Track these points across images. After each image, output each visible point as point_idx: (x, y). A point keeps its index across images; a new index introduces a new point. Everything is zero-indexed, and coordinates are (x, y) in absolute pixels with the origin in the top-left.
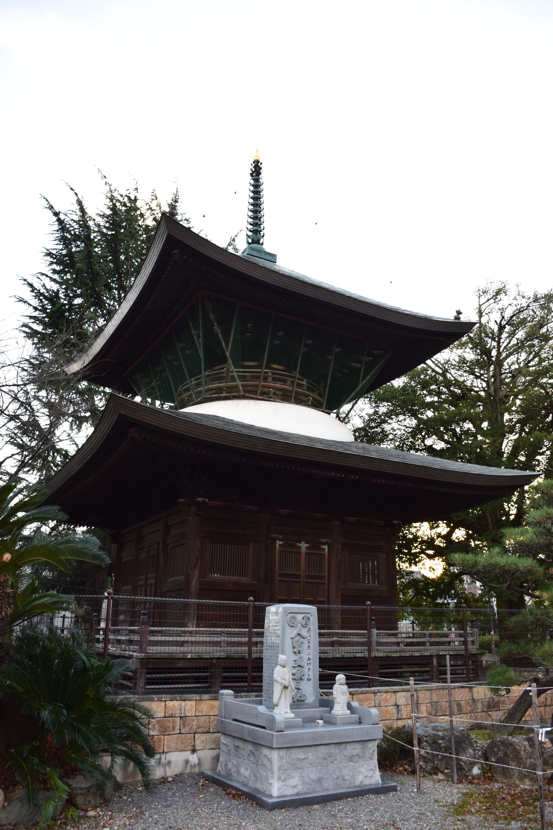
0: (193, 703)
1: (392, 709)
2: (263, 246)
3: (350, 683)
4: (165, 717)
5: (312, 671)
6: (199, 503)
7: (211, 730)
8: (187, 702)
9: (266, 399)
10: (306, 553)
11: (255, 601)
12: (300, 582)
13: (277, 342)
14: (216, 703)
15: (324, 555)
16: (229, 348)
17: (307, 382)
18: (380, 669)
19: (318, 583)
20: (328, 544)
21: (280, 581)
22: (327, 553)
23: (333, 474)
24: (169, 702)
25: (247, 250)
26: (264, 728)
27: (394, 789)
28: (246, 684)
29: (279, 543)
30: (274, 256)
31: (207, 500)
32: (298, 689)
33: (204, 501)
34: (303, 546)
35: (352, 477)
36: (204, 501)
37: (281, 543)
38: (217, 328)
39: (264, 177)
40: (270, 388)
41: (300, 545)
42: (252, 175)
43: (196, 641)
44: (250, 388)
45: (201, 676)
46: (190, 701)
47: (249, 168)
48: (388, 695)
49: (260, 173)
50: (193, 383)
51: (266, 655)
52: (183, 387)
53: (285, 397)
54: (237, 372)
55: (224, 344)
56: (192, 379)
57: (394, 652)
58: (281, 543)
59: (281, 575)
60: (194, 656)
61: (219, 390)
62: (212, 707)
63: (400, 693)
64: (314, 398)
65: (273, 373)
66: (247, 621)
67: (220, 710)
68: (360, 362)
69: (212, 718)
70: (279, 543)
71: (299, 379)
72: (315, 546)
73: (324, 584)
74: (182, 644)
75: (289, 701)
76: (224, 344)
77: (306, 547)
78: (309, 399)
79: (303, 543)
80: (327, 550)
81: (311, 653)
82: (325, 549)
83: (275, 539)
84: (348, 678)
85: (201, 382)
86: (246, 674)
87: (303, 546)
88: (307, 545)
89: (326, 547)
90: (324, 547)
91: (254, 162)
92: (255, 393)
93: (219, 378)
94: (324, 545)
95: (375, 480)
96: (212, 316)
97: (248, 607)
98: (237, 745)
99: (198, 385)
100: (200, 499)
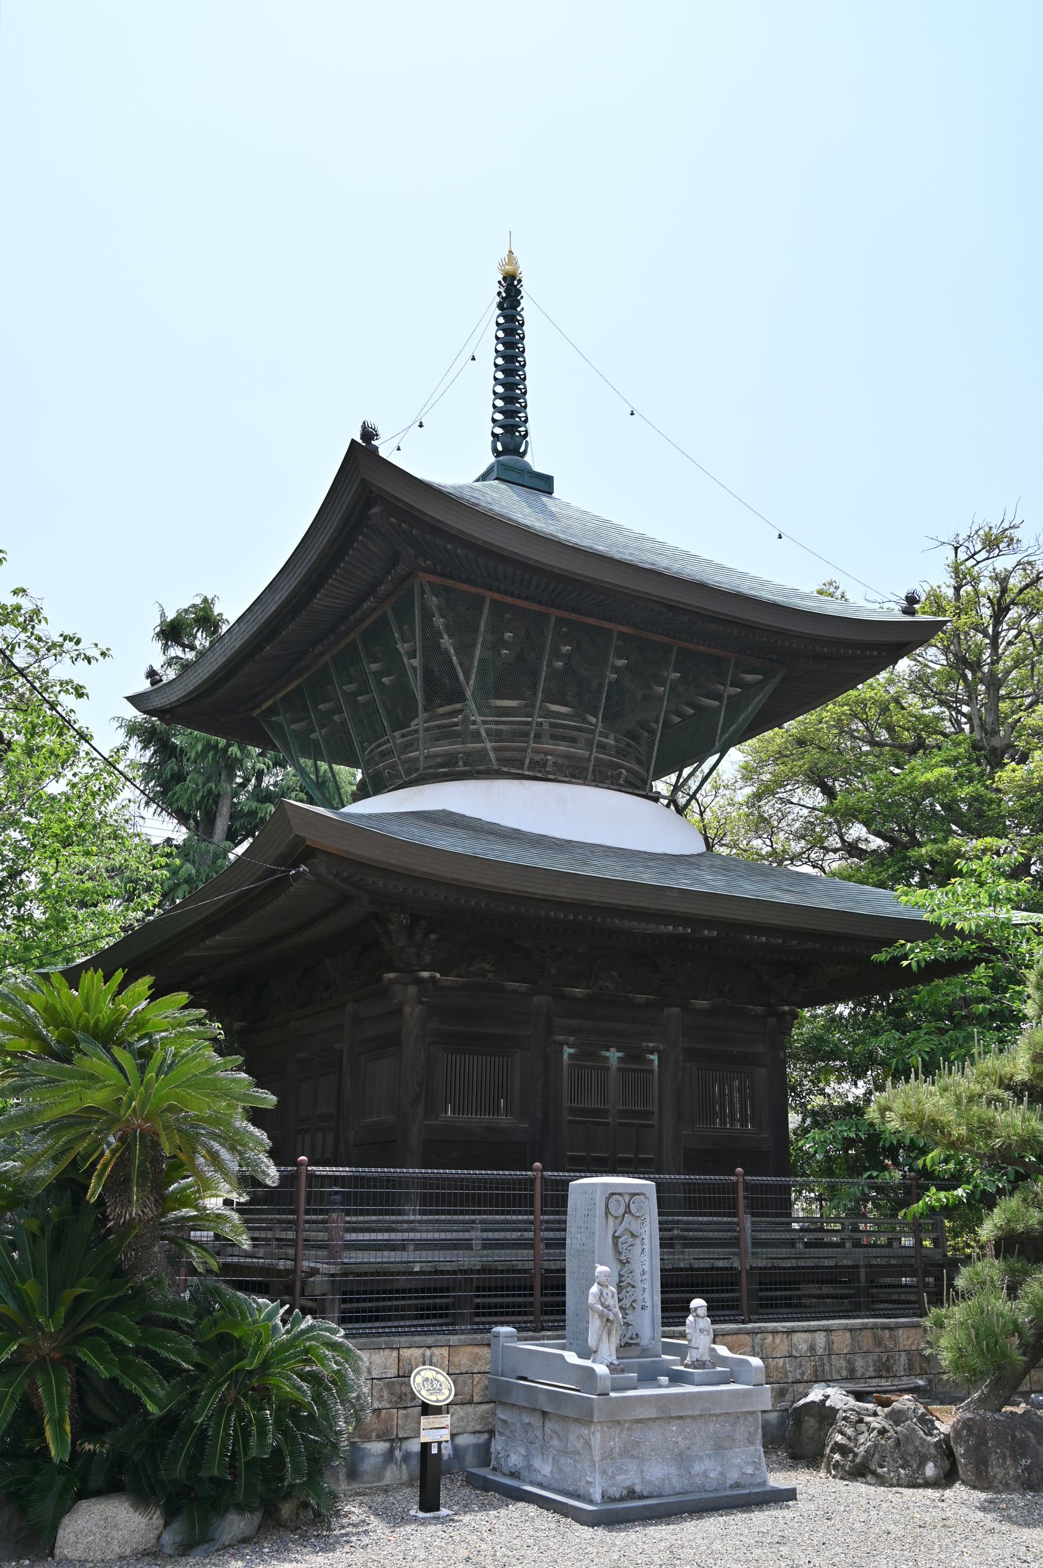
0: (445, 1351)
1: (784, 1363)
3: (715, 1312)
4: (399, 1376)
5: (650, 1293)
6: (422, 981)
7: (476, 1399)
8: (434, 1349)
9: (539, 775)
10: (619, 1069)
11: (545, 1169)
12: (607, 1124)
13: (560, 664)
14: (485, 1352)
15: (652, 1072)
17: (616, 740)
18: (761, 1290)
19: (642, 1125)
21: (570, 1122)
22: (656, 1069)
23: (671, 927)
24: (405, 1350)
25: (495, 468)
27: (790, 1495)
28: (531, 1318)
29: (568, 1051)
31: (438, 975)
32: (627, 1324)
33: (432, 978)
34: (614, 1055)
36: (432, 978)
37: (572, 1051)
38: (446, 641)
39: (527, 307)
40: (546, 754)
41: (607, 1054)
42: (500, 306)
43: (415, 1242)
44: (508, 754)
45: (435, 1305)
46: (439, 1349)
47: (491, 292)
49: (519, 304)
50: (398, 741)
51: (571, 1265)
52: (378, 746)
54: (484, 722)
55: (461, 676)
56: (397, 734)
57: (785, 1259)
58: (572, 1051)
59: (573, 1111)
60: (427, 1268)
61: (450, 760)
62: (477, 1358)
63: (798, 1334)
64: (628, 770)
65: (551, 725)
66: (532, 1206)
67: (494, 1361)
68: (718, 697)
69: (477, 1377)
70: (568, 1051)
71: (602, 734)
72: (635, 1057)
73: (652, 1126)
74: (402, 1246)
75: (615, 1341)
76: (461, 676)
77: (619, 1058)
78: (621, 773)
79: (613, 1050)
80: (656, 1063)
81: (647, 1261)
82: (652, 1061)
83: (561, 1044)
85: (417, 739)
86: (539, 1299)
87: (614, 1055)
88: (620, 1054)
89: (655, 1057)
90: (652, 1057)
91: (504, 279)
92: (520, 763)
93: (446, 734)
94: (652, 1053)
95: (748, 937)
96: (439, 621)
97: (532, 1181)
98: (526, 1421)
99: (408, 747)
100: (425, 974)
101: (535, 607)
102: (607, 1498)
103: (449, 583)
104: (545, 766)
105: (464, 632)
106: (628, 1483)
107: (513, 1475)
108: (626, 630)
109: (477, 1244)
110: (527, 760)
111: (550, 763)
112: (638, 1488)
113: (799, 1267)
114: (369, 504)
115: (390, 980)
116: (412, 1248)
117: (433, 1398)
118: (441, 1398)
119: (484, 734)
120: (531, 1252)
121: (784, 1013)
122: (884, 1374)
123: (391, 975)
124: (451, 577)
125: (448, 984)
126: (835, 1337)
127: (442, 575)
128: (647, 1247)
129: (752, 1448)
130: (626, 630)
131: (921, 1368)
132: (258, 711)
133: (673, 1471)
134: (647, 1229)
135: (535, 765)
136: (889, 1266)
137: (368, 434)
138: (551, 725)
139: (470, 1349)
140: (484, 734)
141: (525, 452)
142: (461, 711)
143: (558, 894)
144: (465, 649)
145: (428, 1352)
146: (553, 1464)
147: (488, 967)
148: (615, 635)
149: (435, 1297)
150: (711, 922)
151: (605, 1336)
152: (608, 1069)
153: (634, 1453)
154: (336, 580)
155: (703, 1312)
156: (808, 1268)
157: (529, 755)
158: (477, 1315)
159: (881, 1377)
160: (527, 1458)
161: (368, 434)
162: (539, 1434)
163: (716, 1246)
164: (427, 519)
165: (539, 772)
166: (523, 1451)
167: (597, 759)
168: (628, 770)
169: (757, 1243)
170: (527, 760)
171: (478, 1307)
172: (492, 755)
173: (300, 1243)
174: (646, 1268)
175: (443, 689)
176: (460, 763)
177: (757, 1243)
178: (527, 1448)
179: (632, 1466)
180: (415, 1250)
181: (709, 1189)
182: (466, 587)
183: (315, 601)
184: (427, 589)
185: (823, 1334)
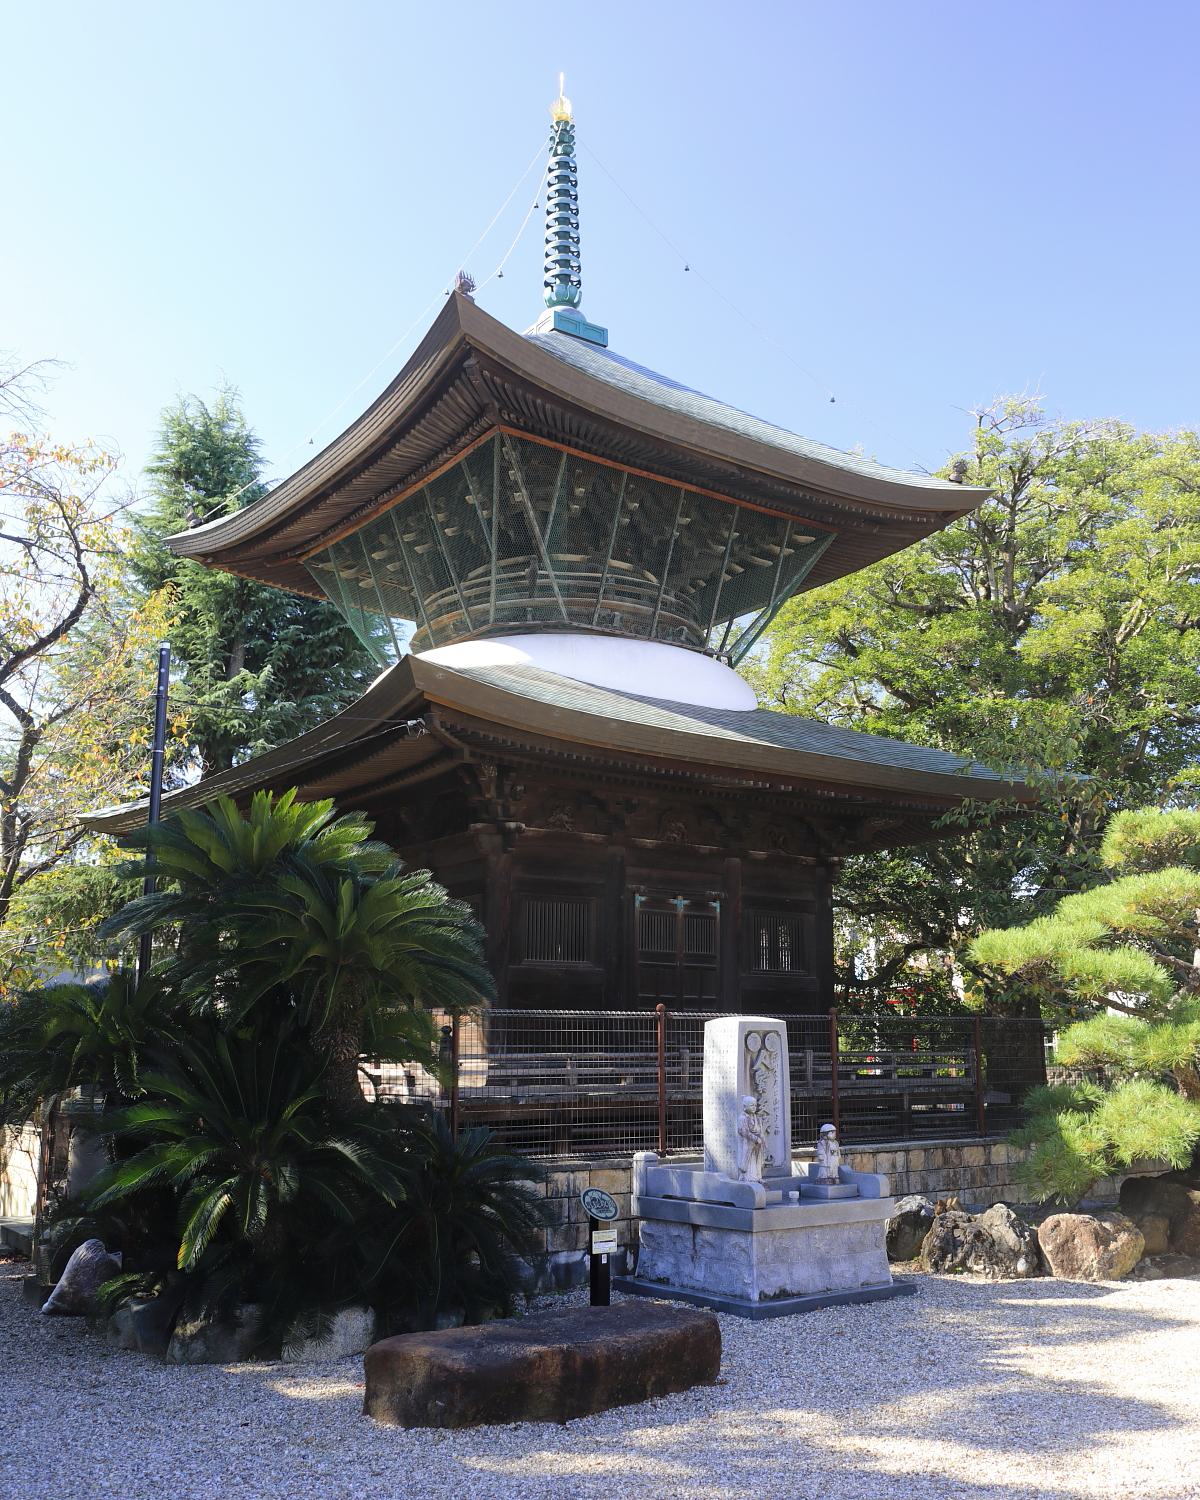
2: (578, 309)
8: (577, 1173)
10: (685, 916)
12: (674, 967)
15: (715, 918)
16: (547, 537)
20: (721, 900)
21: (641, 965)
26: (732, 1205)
29: (639, 899)
30: (603, 332)
31: (523, 826)
33: (518, 829)
34: (681, 903)
35: (783, 787)
36: (518, 829)
37: (643, 899)
41: (675, 902)
44: (575, 609)
48: (866, 1158)
53: (639, 629)
54: (557, 577)
58: (643, 899)
64: (690, 628)
72: (699, 904)
73: (714, 969)
79: (680, 898)
84: (840, 1131)
87: (681, 903)
88: (686, 902)
89: (717, 905)
90: (714, 904)
92: (589, 619)
100: (512, 825)
101: (609, 463)
102: (763, 1296)
103: (529, 436)
104: (612, 622)
105: (538, 482)
106: (780, 1284)
107: (660, 1281)
108: (693, 489)
109: (573, 1080)
110: (596, 616)
111: (617, 619)
112: (788, 1288)
113: (854, 1097)
114: (466, 355)
115: (476, 830)
116: (516, 1083)
117: (603, 1215)
118: (609, 1215)
119: (556, 589)
120: (830, 1082)
121: (834, 864)
122: (951, 1187)
123: (479, 825)
124: (532, 431)
125: (530, 834)
126: (913, 1156)
127: (524, 429)
128: (779, 1079)
129: (879, 1251)
130: (693, 489)
131: (981, 1181)
132: (305, 558)
133: (817, 1272)
134: (779, 1062)
135: (603, 620)
136: (930, 1094)
137: (466, 285)
138: (618, 581)
139: (607, 1172)
140: (556, 589)
141: (579, 302)
142: (526, 564)
143: (655, 750)
144: (541, 500)
145: (572, 1176)
146: (706, 1269)
147: (565, 818)
148: (683, 493)
149: (514, 1129)
150: (786, 779)
151: (754, 1157)
152: (676, 916)
153: (784, 1257)
154: (419, 432)
155: (832, 1135)
156: (862, 1097)
157: (599, 612)
158: (575, 1143)
159: (949, 1190)
160: (676, 1265)
161: (466, 285)
162: (689, 1244)
163: (536, 1082)
164: (520, 373)
165: (607, 627)
166: (672, 1260)
167: (661, 615)
168: (690, 628)
169: (817, 1076)
170: (596, 616)
171: (575, 1137)
172: (563, 610)
173: (835, 1074)
174: (779, 1098)
175: (518, 543)
176: (529, 617)
177: (817, 1076)
178: (676, 1258)
179: (783, 1269)
180: (519, 1085)
181: (569, 1023)
182: (545, 442)
183: (394, 451)
184: (508, 442)
185: (902, 1153)
